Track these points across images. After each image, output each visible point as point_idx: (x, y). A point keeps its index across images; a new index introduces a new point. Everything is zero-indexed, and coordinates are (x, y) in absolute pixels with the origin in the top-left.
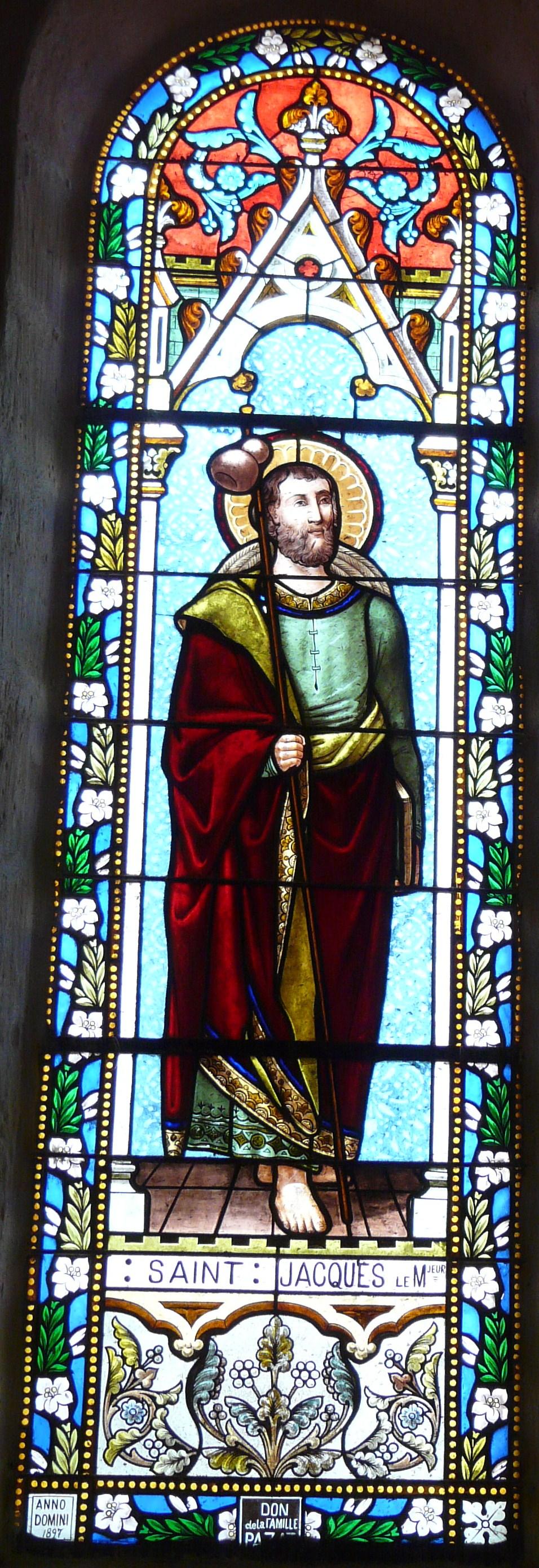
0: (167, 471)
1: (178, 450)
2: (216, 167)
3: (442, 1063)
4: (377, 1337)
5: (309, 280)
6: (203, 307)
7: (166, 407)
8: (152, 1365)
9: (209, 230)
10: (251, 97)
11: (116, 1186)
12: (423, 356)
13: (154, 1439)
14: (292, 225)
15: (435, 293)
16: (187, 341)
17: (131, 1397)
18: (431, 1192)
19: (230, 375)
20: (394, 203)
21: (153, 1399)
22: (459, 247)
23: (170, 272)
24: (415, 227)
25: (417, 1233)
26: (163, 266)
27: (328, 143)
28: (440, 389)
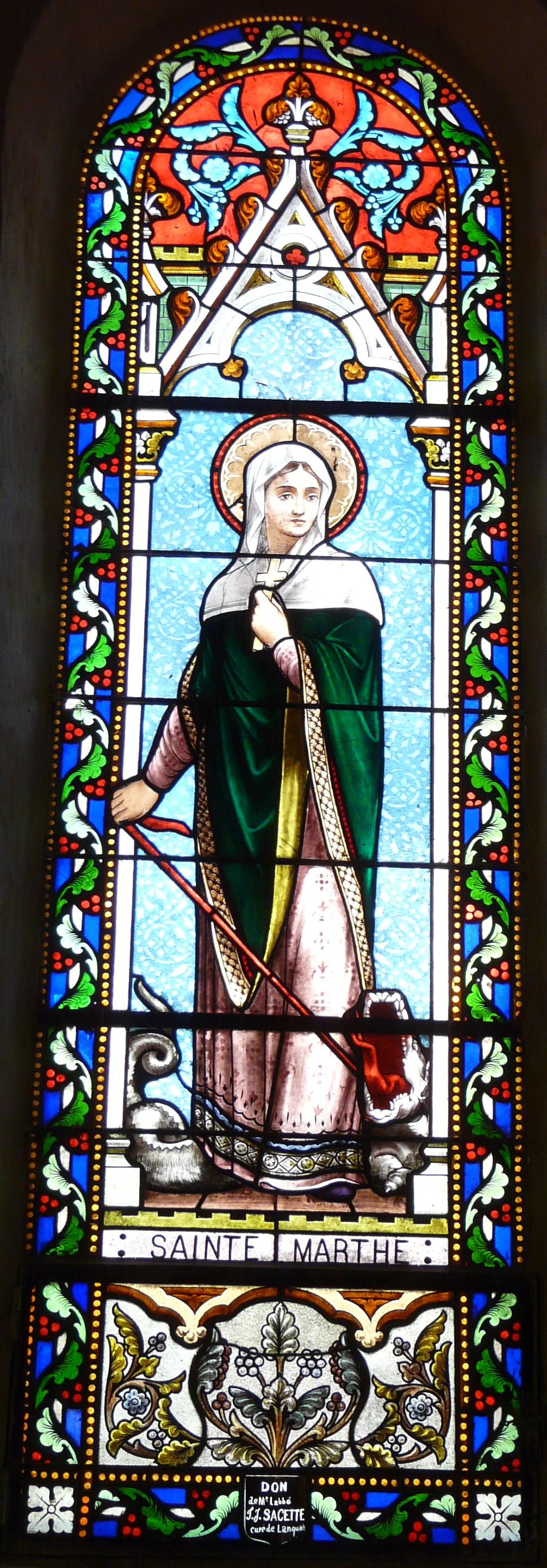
0: (160, 453)
1: (170, 433)
2: (203, 157)
3: (441, 1037)
4: (386, 1326)
5: (294, 268)
6: (190, 294)
7: (157, 393)
8: (155, 1353)
9: (196, 220)
10: (235, 91)
11: (110, 1160)
12: (412, 338)
13: (158, 1430)
14: (278, 214)
15: (424, 279)
16: (177, 329)
17: (131, 1387)
18: (434, 1168)
19: (221, 360)
20: (379, 190)
21: (157, 1389)
22: (444, 231)
23: (160, 264)
24: (399, 215)
25: (419, 1209)
26: (151, 258)
27: (312, 135)
28: (430, 373)
